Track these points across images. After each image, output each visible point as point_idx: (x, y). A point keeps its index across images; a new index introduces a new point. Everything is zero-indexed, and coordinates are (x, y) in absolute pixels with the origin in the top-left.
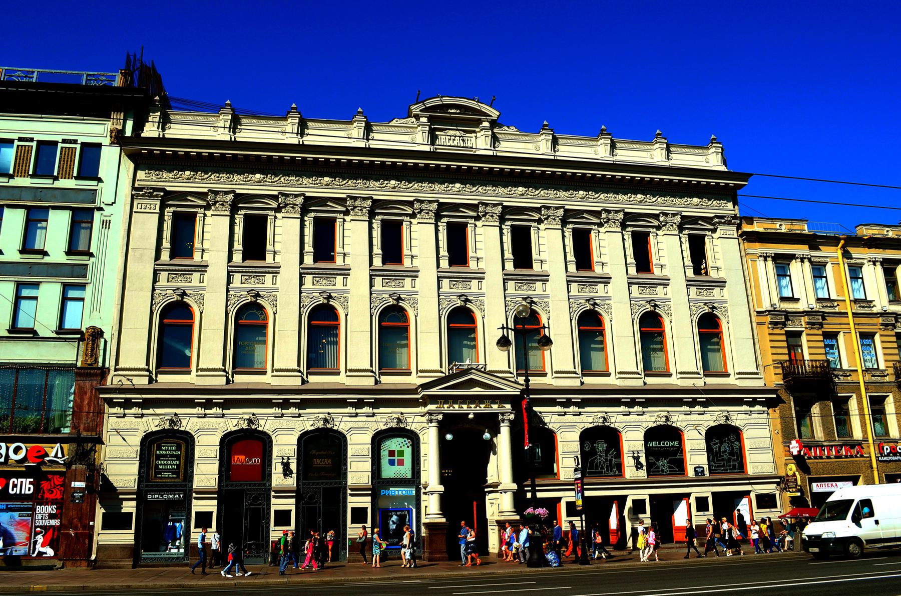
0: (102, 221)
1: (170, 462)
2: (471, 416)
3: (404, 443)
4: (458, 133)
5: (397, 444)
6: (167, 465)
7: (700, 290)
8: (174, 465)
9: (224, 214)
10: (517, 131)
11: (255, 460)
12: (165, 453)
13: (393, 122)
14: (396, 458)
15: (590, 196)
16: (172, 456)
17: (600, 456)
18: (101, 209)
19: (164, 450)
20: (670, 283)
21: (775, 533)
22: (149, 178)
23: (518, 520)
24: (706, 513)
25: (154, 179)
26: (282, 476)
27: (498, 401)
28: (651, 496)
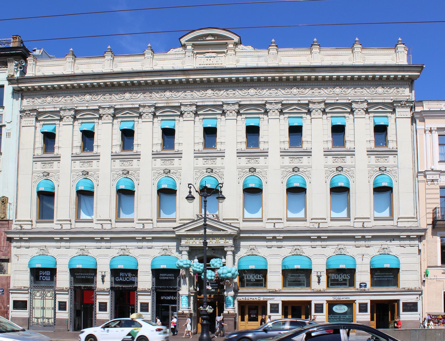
4: (214, 55)
7: (378, 158)
15: (301, 93)
18: (5, 126)
20: (183, 156)
22: (29, 105)
25: (32, 104)
27: (224, 238)
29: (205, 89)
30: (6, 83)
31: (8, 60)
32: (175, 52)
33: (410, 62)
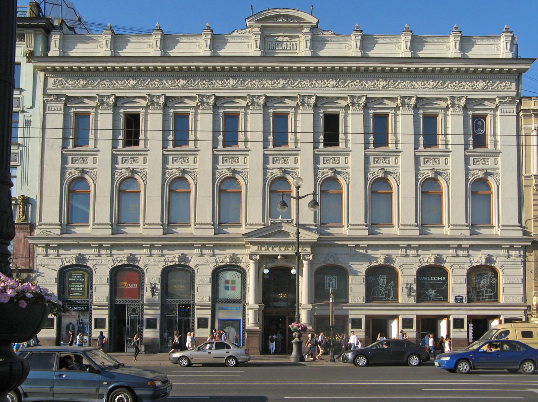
1: (78, 286)
2: (279, 257)
5: (231, 275)
6: (78, 287)
9: (109, 112)
10: (333, 34)
12: (75, 280)
14: (230, 285)
16: (79, 282)
19: (74, 278)
21: (16, 344)
23: (311, 330)
24: (462, 330)
26: (406, 296)
28: (418, 316)
29: (76, 78)
31: (26, 32)
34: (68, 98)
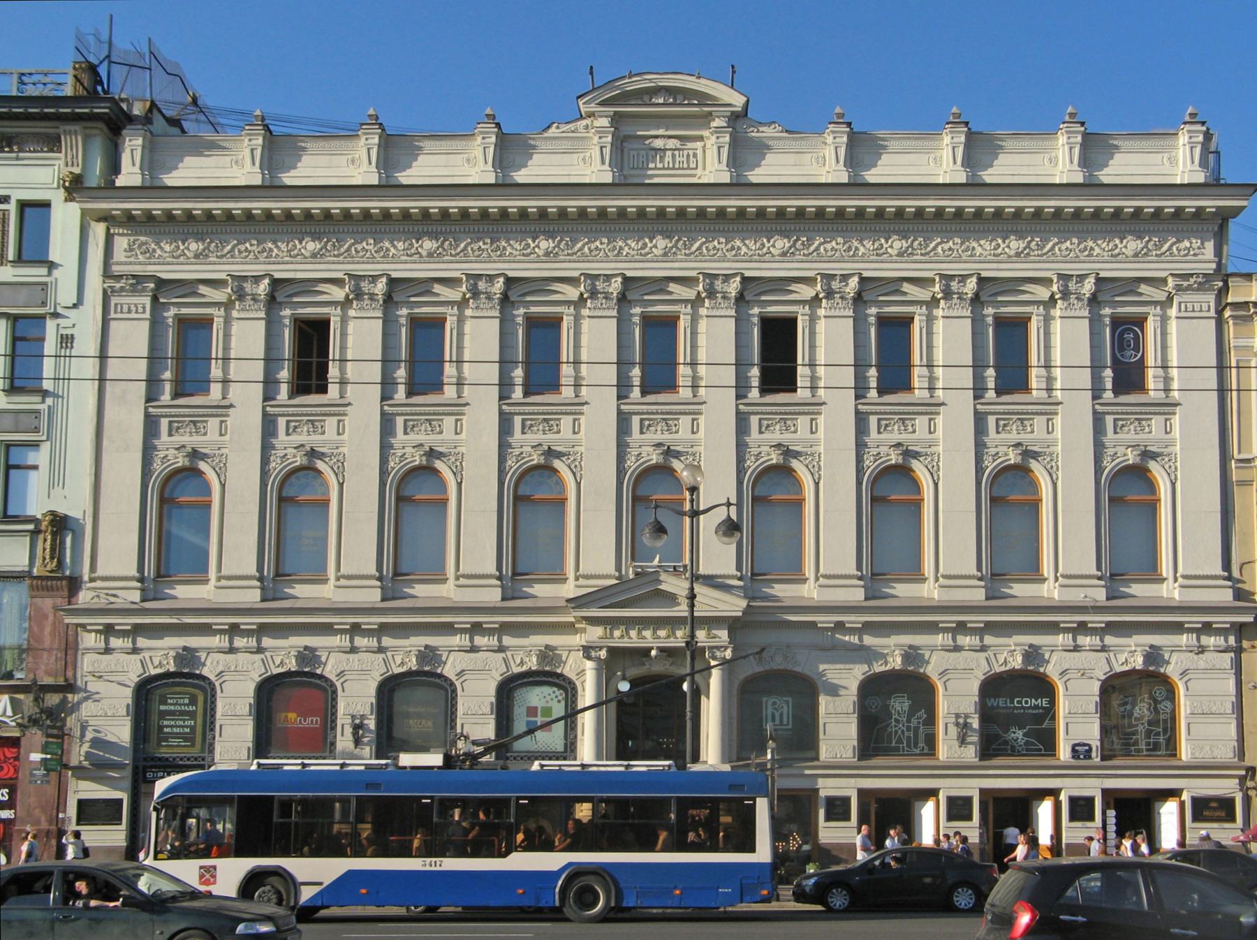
0: (59, 336)
1: (181, 723)
3: (554, 695)
5: (541, 696)
6: (180, 726)
8: (187, 727)
10: (782, 132)
11: (312, 720)
13: (550, 131)
16: (182, 713)
17: (897, 721)
19: (171, 704)
24: (1089, 824)
26: (956, 743)
30: (57, 197)
31: (65, 131)
32: (564, 132)
33: (1184, 179)
34: (161, 284)
